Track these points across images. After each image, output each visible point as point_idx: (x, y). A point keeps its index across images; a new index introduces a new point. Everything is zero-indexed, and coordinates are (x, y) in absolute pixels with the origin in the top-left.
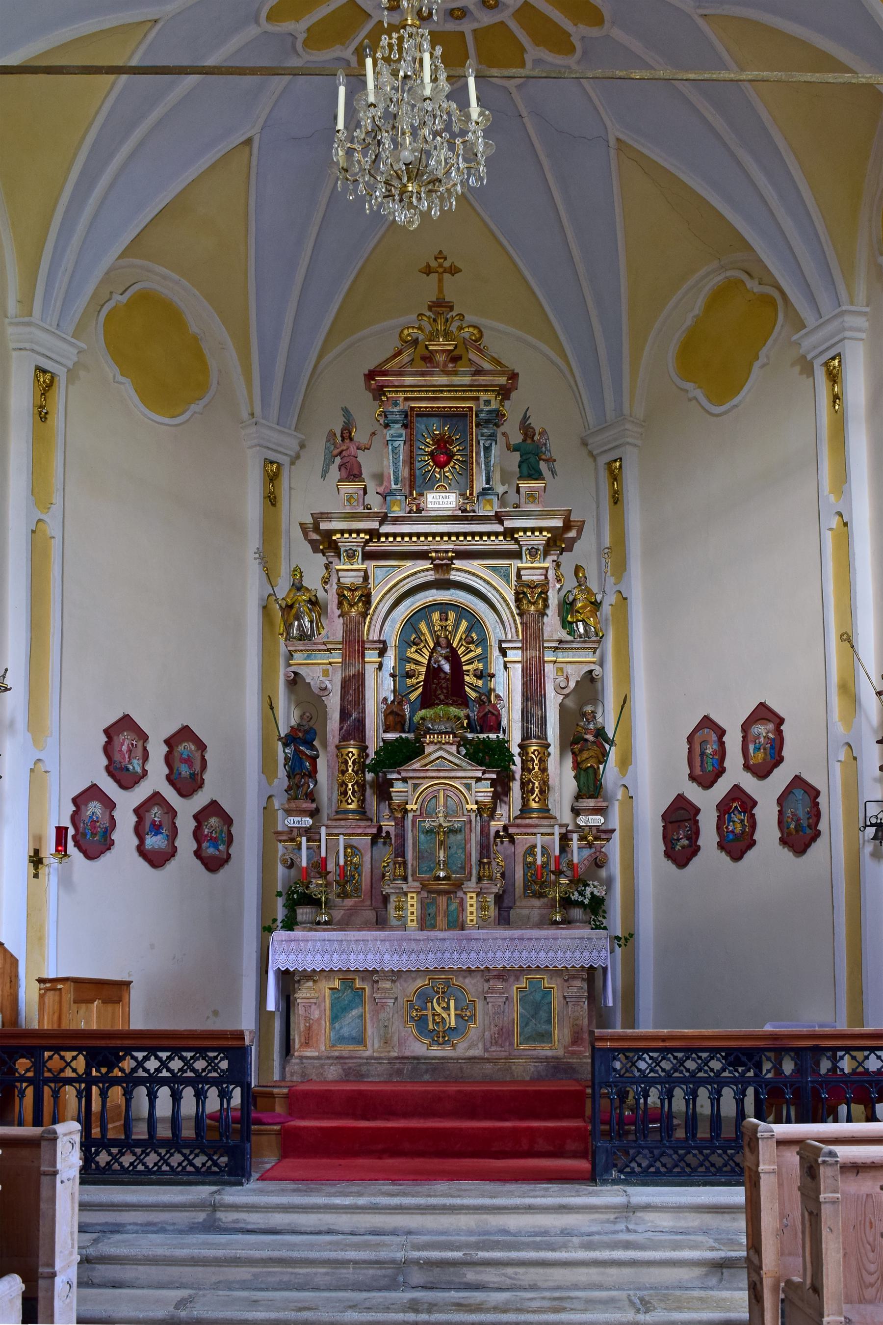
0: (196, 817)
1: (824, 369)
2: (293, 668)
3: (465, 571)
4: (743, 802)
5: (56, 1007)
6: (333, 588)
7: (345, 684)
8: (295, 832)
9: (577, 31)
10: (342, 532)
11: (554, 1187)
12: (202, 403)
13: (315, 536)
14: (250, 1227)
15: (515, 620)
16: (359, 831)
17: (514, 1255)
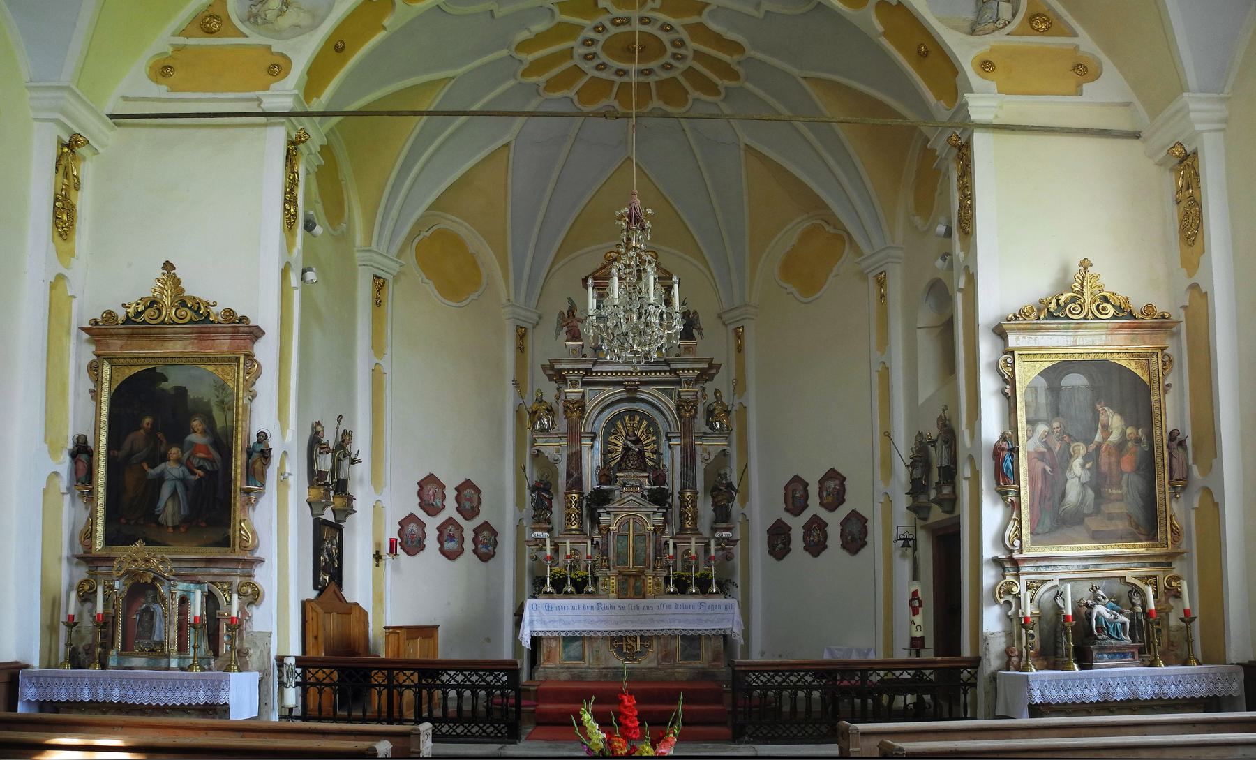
7: (569, 458)
9: (722, 83)
10: (568, 370)
11: (710, 745)
13: (551, 372)
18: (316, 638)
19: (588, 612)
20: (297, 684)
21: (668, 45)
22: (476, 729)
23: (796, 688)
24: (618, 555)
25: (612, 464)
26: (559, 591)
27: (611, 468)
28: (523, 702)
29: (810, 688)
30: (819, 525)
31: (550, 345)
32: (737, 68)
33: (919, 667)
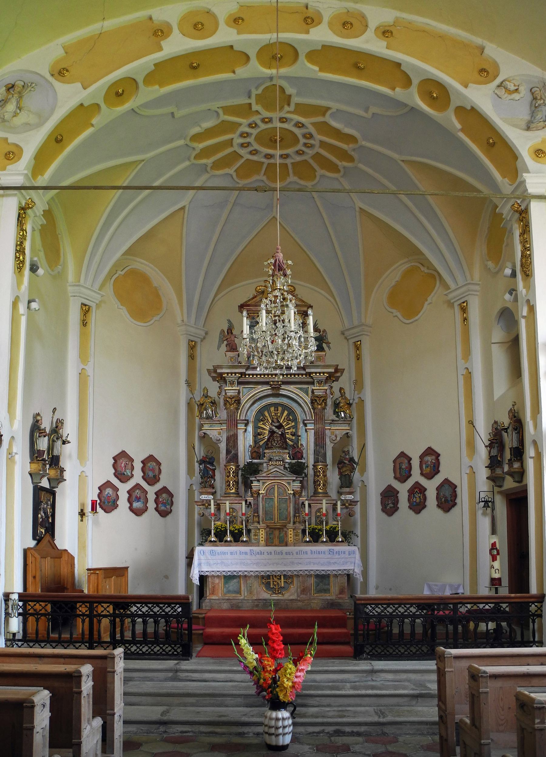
0: (156, 493)
1: (459, 306)
2: (204, 431)
3: (287, 390)
4: (420, 489)
5: (96, 581)
6: (222, 398)
8: (205, 501)
10: (228, 373)
11: (337, 661)
12: (159, 316)
14: (193, 679)
15: (311, 411)
16: (236, 502)
17: (320, 692)
18: (34, 577)
19: (243, 557)
20: (19, 614)
21: (300, 137)
22: (158, 648)
23: (403, 616)
24: (266, 513)
25: (261, 443)
26: (221, 541)
27: (260, 447)
28: (194, 627)
29: (414, 617)
30: (420, 490)
31: (213, 355)
32: (352, 153)
33: (498, 601)
